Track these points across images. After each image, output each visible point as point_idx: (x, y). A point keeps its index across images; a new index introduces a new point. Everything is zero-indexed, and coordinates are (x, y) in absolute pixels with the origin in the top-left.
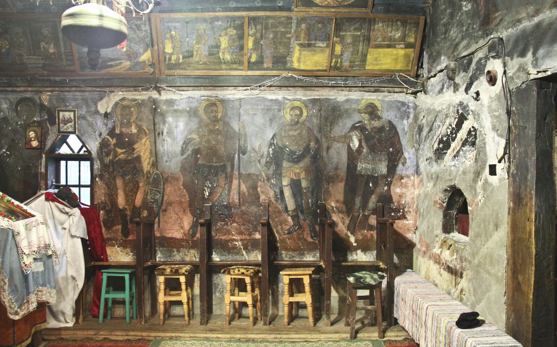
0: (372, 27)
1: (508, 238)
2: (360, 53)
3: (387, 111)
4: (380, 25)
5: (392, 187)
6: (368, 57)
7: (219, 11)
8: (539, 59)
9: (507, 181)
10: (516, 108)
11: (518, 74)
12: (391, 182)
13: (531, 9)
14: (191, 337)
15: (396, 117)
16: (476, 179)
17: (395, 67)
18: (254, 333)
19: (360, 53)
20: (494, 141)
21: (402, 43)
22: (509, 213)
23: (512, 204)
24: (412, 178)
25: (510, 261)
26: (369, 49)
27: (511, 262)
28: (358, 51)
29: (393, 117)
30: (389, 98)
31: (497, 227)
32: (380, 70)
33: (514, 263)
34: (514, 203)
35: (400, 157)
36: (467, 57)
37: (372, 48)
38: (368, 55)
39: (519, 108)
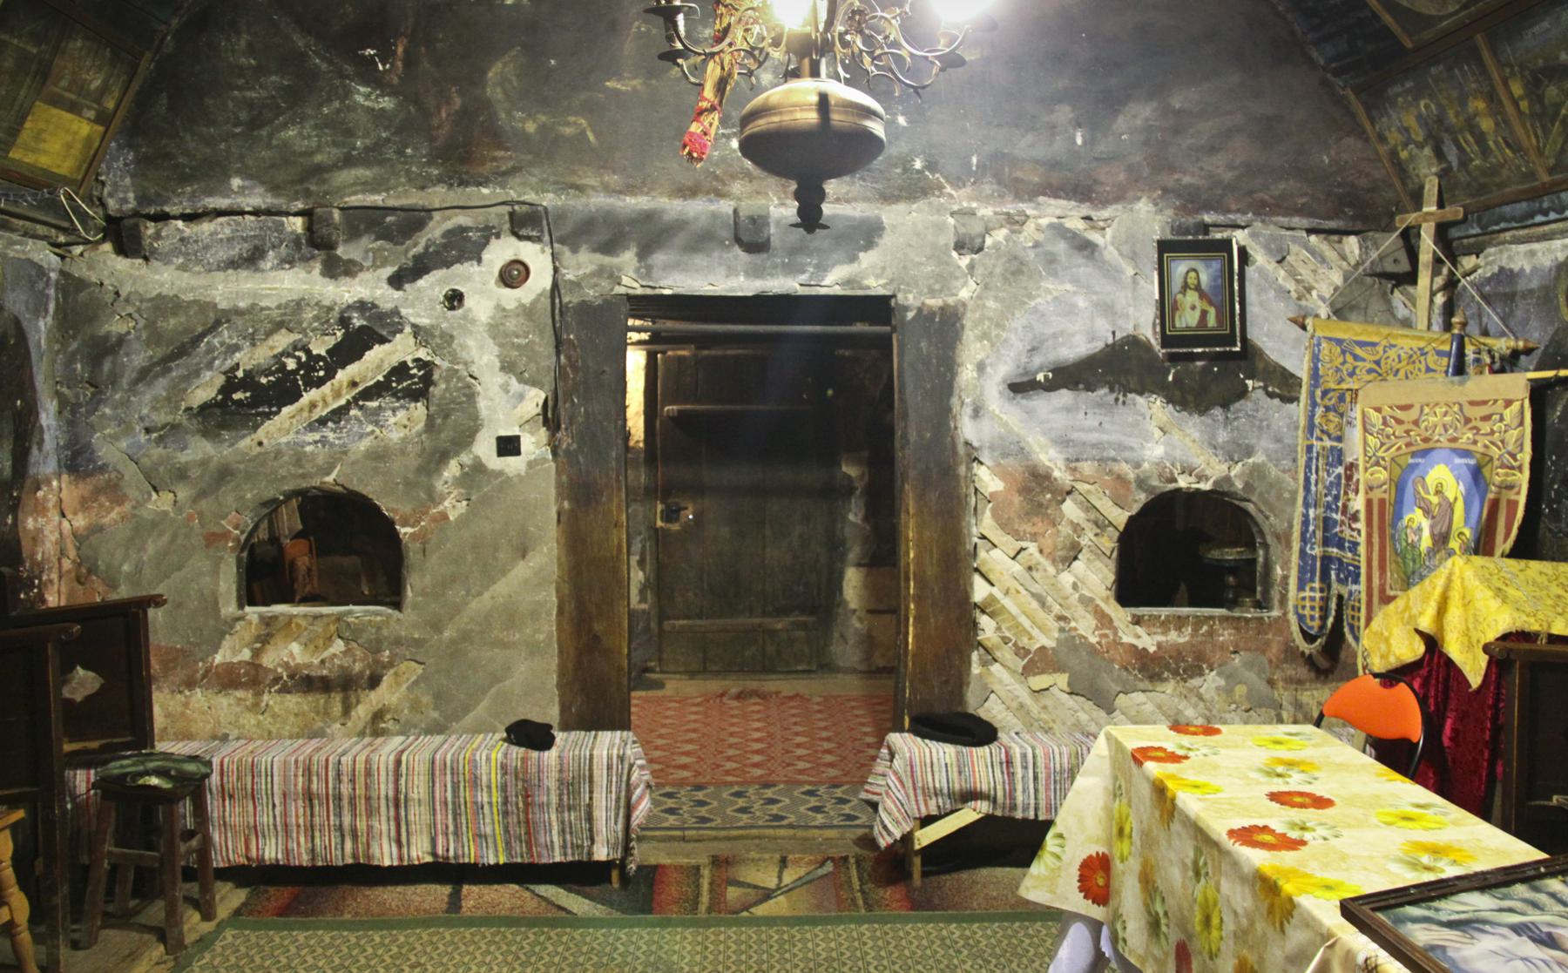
0: (63, 44)
1: (560, 564)
2: (16, 108)
3: (13, 290)
4: (79, 44)
5: (21, 516)
6: (28, 125)
7: (1497, 314)
8: (655, 269)
9: (553, 465)
10: (577, 337)
11: (594, 280)
12: (19, 499)
13: (614, 179)
14: (447, 827)
15: (27, 309)
16: (432, 466)
17: (59, 166)
18: (797, 672)
19: (16, 108)
20: (507, 392)
21: (95, 106)
22: (559, 521)
23: (566, 505)
24: (55, 483)
25: (567, 608)
26: (38, 103)
27: (570, 607)
28: (15, 100)
29: (23, 308)
30: (17, 251)
31: (523, 552)
32: (31, 167)
33: (581, 605)
34: (575, 500)
35: (33, 426)
36: (402, 214)
37: (45, 102)
38: (30, 118)
39: (583, 337)
